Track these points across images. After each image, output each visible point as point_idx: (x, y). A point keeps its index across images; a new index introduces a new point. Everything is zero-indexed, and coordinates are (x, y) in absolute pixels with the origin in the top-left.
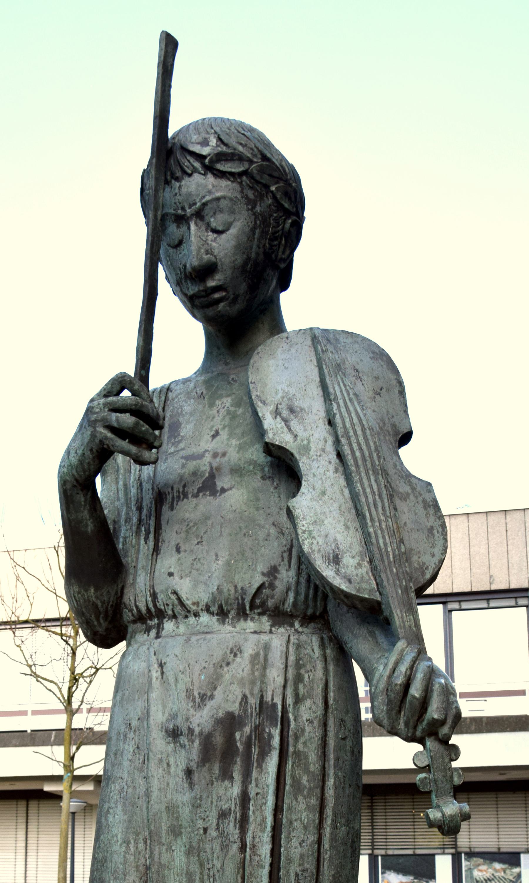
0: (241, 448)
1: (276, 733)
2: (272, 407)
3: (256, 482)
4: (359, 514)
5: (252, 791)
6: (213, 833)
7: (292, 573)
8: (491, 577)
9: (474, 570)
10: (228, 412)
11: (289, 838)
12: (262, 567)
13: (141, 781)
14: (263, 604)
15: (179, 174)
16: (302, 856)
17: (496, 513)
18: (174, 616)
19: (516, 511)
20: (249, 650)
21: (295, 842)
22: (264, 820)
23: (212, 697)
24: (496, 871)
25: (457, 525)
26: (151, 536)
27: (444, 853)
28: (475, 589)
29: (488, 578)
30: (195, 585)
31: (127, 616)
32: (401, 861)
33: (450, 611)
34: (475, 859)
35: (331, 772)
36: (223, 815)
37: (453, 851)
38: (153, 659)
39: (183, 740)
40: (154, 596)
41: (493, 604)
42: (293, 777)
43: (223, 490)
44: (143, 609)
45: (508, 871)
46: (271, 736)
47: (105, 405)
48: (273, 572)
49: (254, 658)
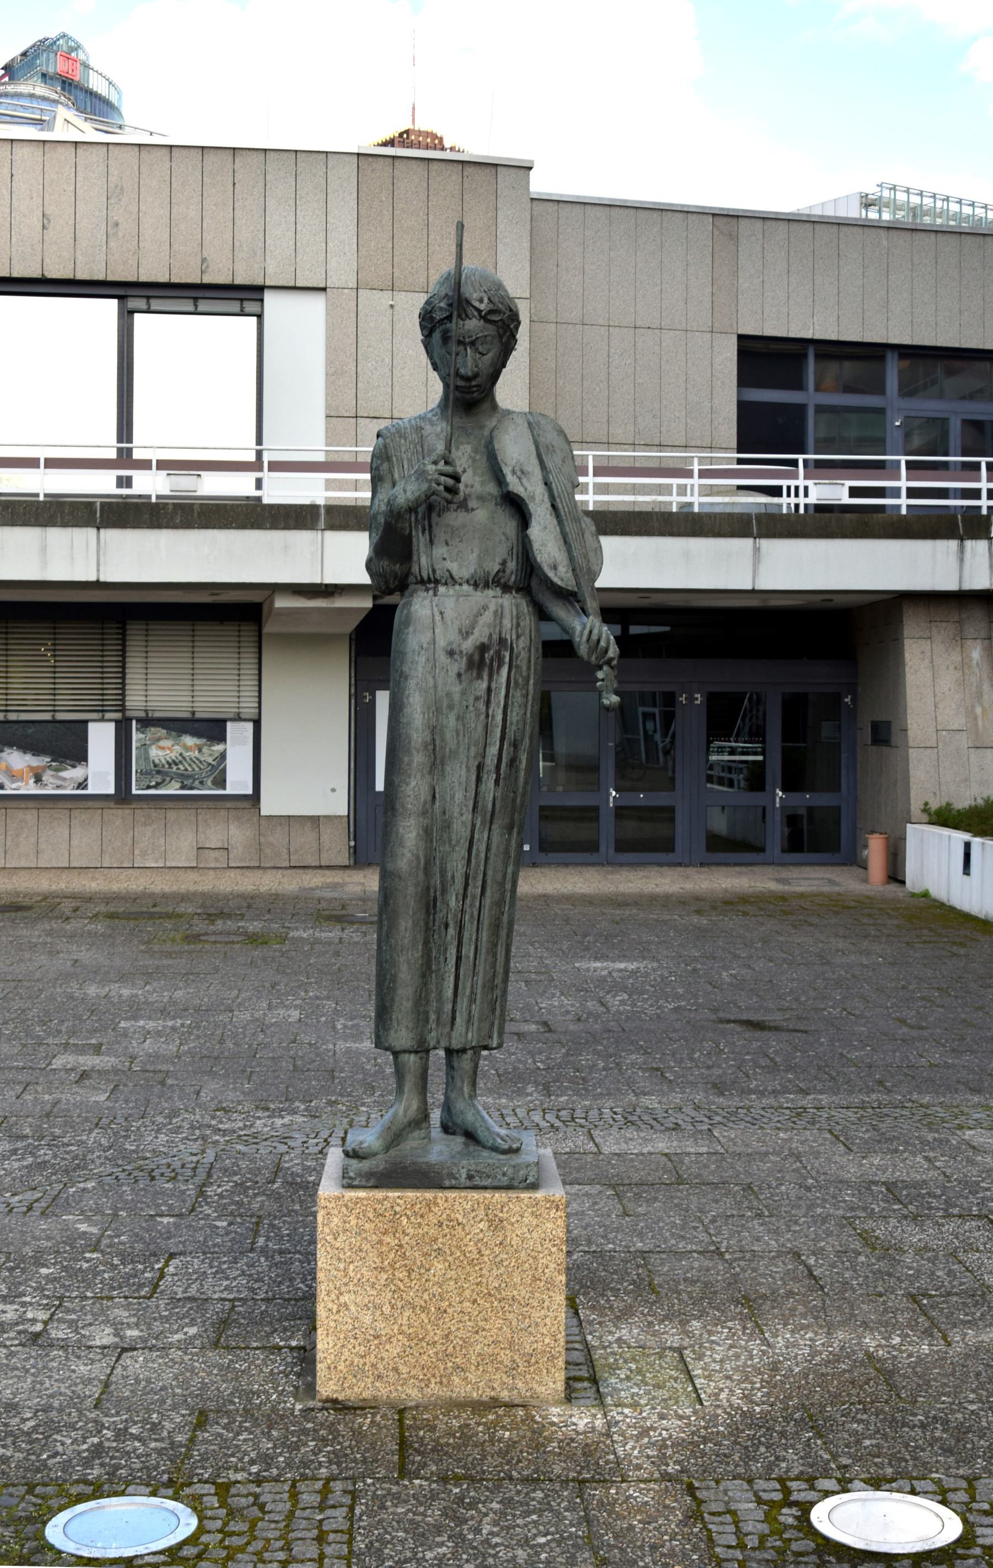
0: (482, 483)
1: (507, 655)
2: (510, 468)
3: (491, 506)
4: (566, 542)
5: (494, 685)
6: (471, 708)
7: (514, 563)
8: (204, 260)
9: (175, 247)
10: (471, 457)
11: (512, 711)
12: (498, 560)
13: (431, 679)
14: (499, 580)
15: (464, 316)
16: (517, 722)
17: (219, 151)
18: (446, 584)
19: (252, 152)
20: (492, 607)
21: (514, 714)
22: (499, 701)
23: (472, 633)
24: (187, 749)
25: (152, 164)
26: (427, 532)
27: (102, 720)
28: (175, 280)
29: (200, 263)
30: (460, 567)
31: (411, 579)
32: (30, 731)
33: (131, 312)
34: (153, 729)
35: (532, 676)
36: (477, 699)
37: (118, 716)
38: (435, 609)
39: (456, 657)
40: (434, 571)
41: (202, 306)
42: (515, 679)
43: (473, 510)
44: (425, 577)
45: (205, 750)
46: (504, 656)
47: (436, 470)
48: (504, 563)
49: (496, 612)
